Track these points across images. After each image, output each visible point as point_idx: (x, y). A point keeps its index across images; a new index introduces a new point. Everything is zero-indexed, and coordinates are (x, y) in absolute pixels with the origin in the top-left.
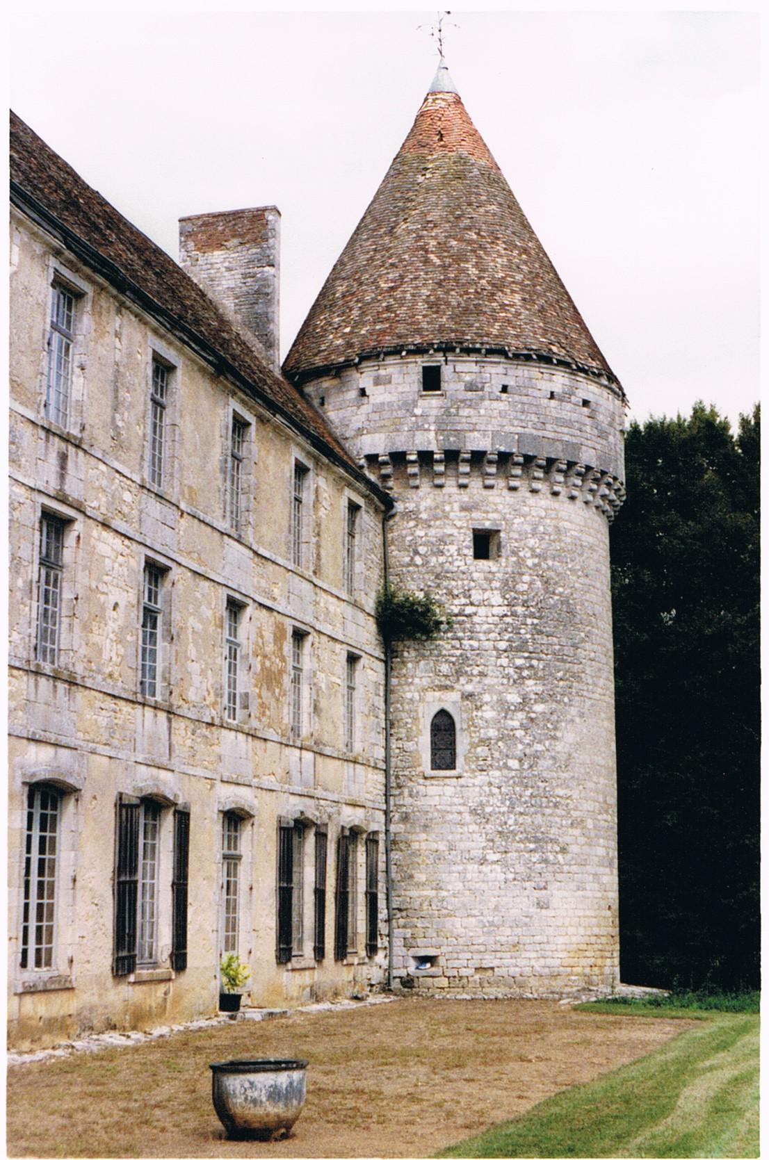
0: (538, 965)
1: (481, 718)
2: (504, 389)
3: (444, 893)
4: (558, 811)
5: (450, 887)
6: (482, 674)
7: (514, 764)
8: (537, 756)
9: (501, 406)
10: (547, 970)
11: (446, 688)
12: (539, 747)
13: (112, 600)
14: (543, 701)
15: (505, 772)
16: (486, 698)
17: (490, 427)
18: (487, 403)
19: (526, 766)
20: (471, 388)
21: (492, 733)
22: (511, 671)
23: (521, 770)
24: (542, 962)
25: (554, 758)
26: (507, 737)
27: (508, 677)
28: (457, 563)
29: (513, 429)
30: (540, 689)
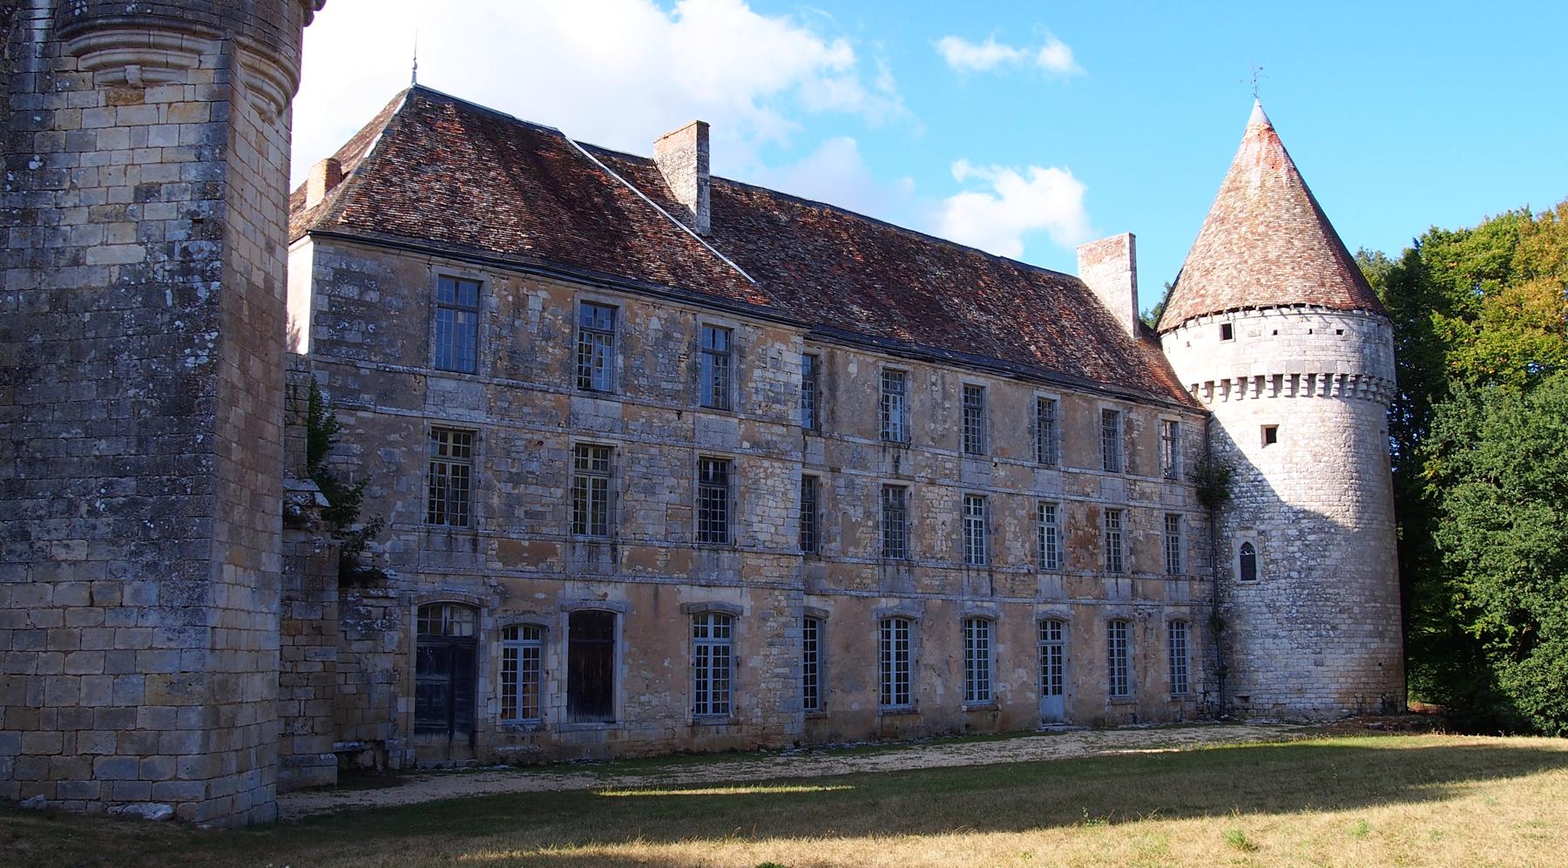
8: (1310, 569)
11: (1248, 528)
13: (940, 520)
20: (1252, 335)
21: (1279, 556)
26: (1291, 559)
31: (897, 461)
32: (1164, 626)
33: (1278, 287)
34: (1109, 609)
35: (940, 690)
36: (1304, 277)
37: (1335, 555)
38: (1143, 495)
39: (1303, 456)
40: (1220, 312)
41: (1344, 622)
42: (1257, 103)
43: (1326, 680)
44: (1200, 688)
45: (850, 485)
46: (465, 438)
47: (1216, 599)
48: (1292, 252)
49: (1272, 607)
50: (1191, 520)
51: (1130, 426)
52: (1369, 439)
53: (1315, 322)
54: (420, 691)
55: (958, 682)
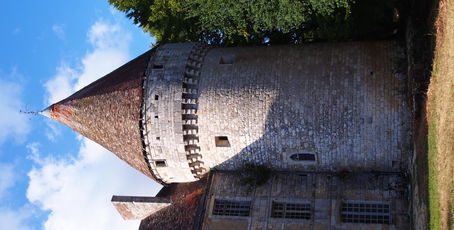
0: (398, 123)
1: (292, 145)
2: (158, 138)
3: (366, 159)
4: (330, 113)
5: (363, 157)
6: (274, 144)
7: (310, 133)
8: (307, 123)
9: (165, 139)
10: (400, 119)
12: (303, 121)
14: (283, 119)
15: (314, 137)
16: (284, 143)
17: (175, 144)
18: (165, 145)
19: (311, 128)
21: (298, 141)
22: (272, 133)
23: (313, 130)
24: (396, 121)
25: (307, 115)
26: (300, 134)
27: (274, 135)
28: (231, 152)
29: (173, 135)
30: (278, 121)
33: (131, 135)
36: (125, 116)
37: (298, 106)
39: (234, 124)
40: (150, 167)
41: (342, 102)
42: (40, 113)
43: (382, 116)
44: (386, 194)
47: (327, 173)
48: (113, 120)
49: (333, 147)
50: (277, 192)
52: (224, 76)
53: (150, 114)
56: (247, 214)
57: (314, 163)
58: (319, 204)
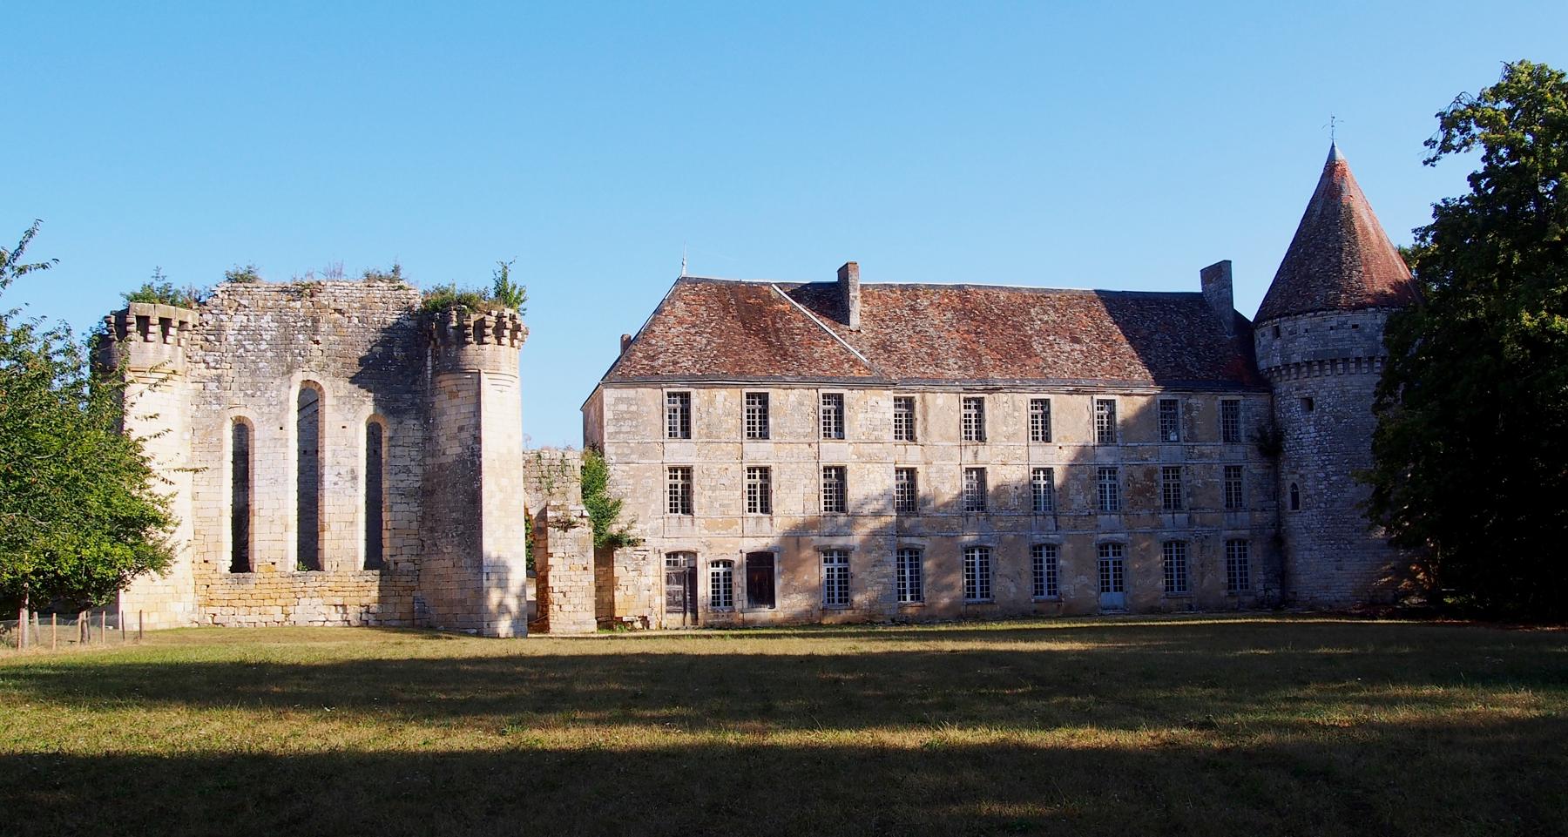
8: (1334, 501)
26: (1321, 494)
31: (976, 453)
32: (1222, 545)
34: (1167, 535)
35: (1013, 590)
38: (1201, 455)
44: (1260, 586)
45: (940, 470)
46: (687, 472)
47: (1278, 522)
50: (1253, 468)
51: (1189, 409)
54: (669, 594)
55: (1028, 584)
56: (1227, 439)
57: (1289, 509)
58: (1244, 516)
